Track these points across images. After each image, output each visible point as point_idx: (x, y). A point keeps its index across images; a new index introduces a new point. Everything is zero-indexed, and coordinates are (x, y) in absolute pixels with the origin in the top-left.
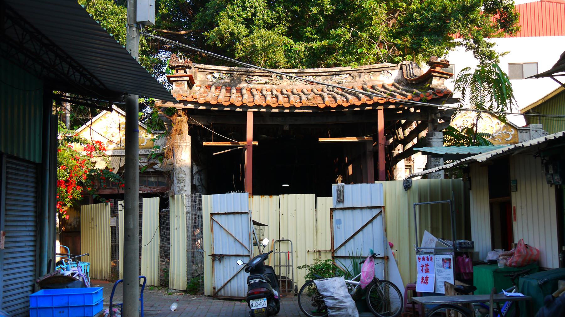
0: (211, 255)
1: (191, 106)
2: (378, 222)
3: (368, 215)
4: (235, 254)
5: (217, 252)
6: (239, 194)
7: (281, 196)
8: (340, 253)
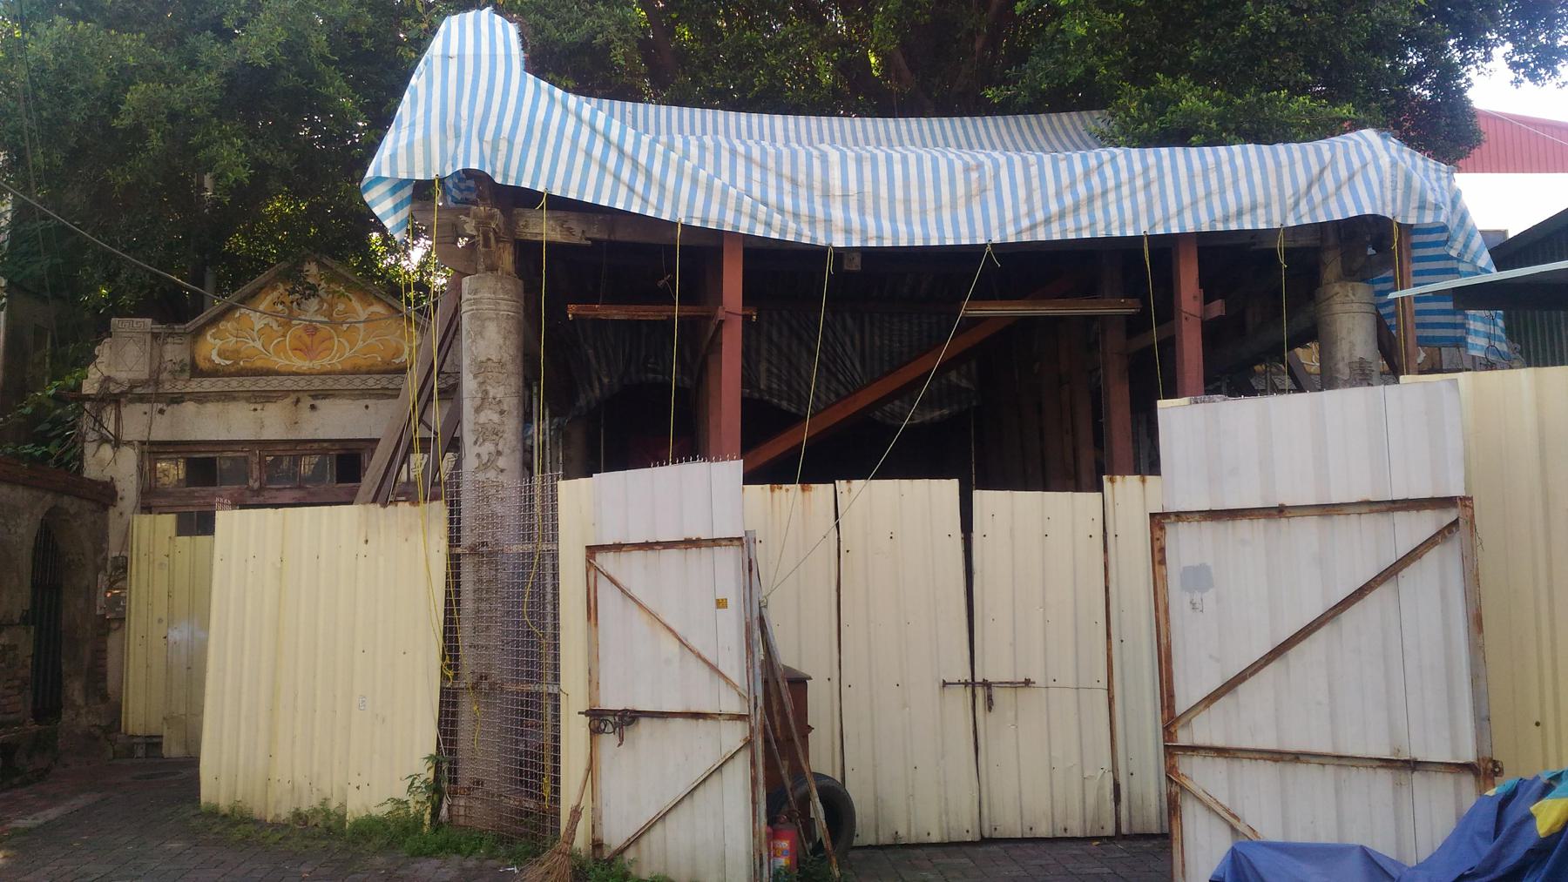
0: (587, 713)
1: (16, 780)
2: (1432, 591)
3: (1361, 549)
4: (1426, 493)
5: (612, 700)
6: (694, 471)
7: (842, 485)
8: (1202, 731)
